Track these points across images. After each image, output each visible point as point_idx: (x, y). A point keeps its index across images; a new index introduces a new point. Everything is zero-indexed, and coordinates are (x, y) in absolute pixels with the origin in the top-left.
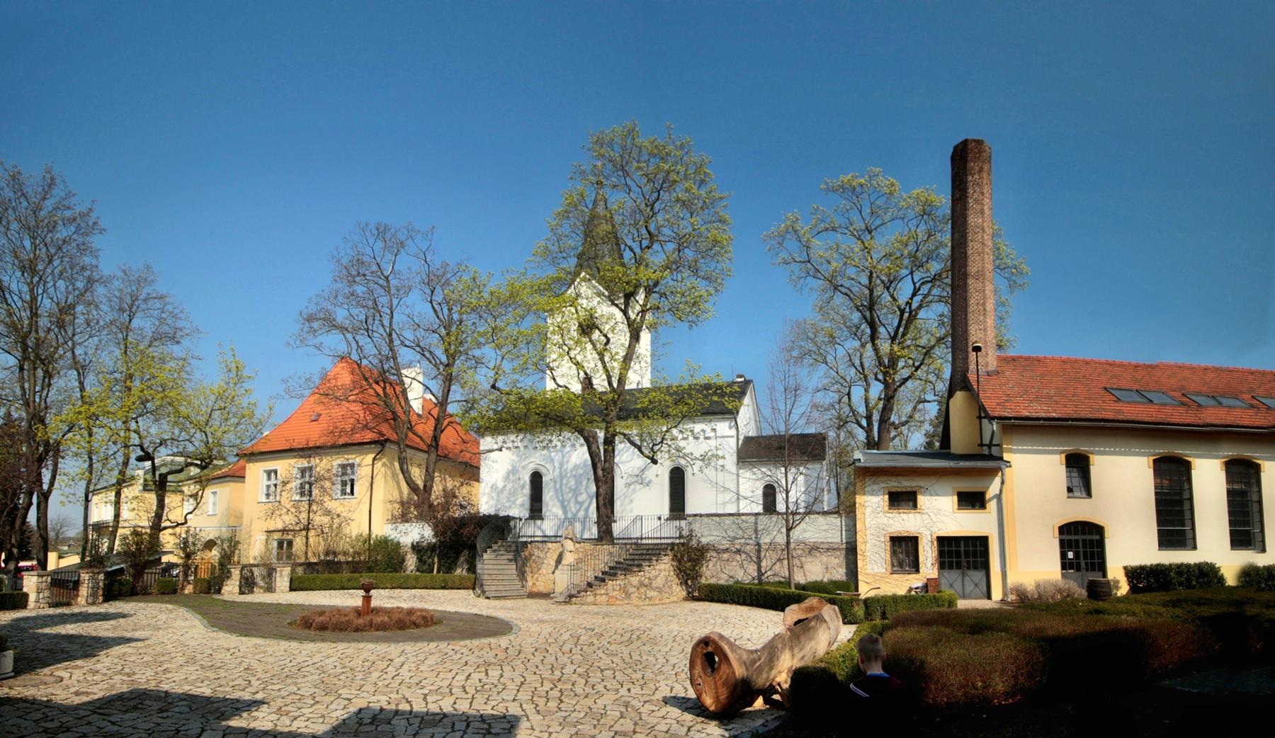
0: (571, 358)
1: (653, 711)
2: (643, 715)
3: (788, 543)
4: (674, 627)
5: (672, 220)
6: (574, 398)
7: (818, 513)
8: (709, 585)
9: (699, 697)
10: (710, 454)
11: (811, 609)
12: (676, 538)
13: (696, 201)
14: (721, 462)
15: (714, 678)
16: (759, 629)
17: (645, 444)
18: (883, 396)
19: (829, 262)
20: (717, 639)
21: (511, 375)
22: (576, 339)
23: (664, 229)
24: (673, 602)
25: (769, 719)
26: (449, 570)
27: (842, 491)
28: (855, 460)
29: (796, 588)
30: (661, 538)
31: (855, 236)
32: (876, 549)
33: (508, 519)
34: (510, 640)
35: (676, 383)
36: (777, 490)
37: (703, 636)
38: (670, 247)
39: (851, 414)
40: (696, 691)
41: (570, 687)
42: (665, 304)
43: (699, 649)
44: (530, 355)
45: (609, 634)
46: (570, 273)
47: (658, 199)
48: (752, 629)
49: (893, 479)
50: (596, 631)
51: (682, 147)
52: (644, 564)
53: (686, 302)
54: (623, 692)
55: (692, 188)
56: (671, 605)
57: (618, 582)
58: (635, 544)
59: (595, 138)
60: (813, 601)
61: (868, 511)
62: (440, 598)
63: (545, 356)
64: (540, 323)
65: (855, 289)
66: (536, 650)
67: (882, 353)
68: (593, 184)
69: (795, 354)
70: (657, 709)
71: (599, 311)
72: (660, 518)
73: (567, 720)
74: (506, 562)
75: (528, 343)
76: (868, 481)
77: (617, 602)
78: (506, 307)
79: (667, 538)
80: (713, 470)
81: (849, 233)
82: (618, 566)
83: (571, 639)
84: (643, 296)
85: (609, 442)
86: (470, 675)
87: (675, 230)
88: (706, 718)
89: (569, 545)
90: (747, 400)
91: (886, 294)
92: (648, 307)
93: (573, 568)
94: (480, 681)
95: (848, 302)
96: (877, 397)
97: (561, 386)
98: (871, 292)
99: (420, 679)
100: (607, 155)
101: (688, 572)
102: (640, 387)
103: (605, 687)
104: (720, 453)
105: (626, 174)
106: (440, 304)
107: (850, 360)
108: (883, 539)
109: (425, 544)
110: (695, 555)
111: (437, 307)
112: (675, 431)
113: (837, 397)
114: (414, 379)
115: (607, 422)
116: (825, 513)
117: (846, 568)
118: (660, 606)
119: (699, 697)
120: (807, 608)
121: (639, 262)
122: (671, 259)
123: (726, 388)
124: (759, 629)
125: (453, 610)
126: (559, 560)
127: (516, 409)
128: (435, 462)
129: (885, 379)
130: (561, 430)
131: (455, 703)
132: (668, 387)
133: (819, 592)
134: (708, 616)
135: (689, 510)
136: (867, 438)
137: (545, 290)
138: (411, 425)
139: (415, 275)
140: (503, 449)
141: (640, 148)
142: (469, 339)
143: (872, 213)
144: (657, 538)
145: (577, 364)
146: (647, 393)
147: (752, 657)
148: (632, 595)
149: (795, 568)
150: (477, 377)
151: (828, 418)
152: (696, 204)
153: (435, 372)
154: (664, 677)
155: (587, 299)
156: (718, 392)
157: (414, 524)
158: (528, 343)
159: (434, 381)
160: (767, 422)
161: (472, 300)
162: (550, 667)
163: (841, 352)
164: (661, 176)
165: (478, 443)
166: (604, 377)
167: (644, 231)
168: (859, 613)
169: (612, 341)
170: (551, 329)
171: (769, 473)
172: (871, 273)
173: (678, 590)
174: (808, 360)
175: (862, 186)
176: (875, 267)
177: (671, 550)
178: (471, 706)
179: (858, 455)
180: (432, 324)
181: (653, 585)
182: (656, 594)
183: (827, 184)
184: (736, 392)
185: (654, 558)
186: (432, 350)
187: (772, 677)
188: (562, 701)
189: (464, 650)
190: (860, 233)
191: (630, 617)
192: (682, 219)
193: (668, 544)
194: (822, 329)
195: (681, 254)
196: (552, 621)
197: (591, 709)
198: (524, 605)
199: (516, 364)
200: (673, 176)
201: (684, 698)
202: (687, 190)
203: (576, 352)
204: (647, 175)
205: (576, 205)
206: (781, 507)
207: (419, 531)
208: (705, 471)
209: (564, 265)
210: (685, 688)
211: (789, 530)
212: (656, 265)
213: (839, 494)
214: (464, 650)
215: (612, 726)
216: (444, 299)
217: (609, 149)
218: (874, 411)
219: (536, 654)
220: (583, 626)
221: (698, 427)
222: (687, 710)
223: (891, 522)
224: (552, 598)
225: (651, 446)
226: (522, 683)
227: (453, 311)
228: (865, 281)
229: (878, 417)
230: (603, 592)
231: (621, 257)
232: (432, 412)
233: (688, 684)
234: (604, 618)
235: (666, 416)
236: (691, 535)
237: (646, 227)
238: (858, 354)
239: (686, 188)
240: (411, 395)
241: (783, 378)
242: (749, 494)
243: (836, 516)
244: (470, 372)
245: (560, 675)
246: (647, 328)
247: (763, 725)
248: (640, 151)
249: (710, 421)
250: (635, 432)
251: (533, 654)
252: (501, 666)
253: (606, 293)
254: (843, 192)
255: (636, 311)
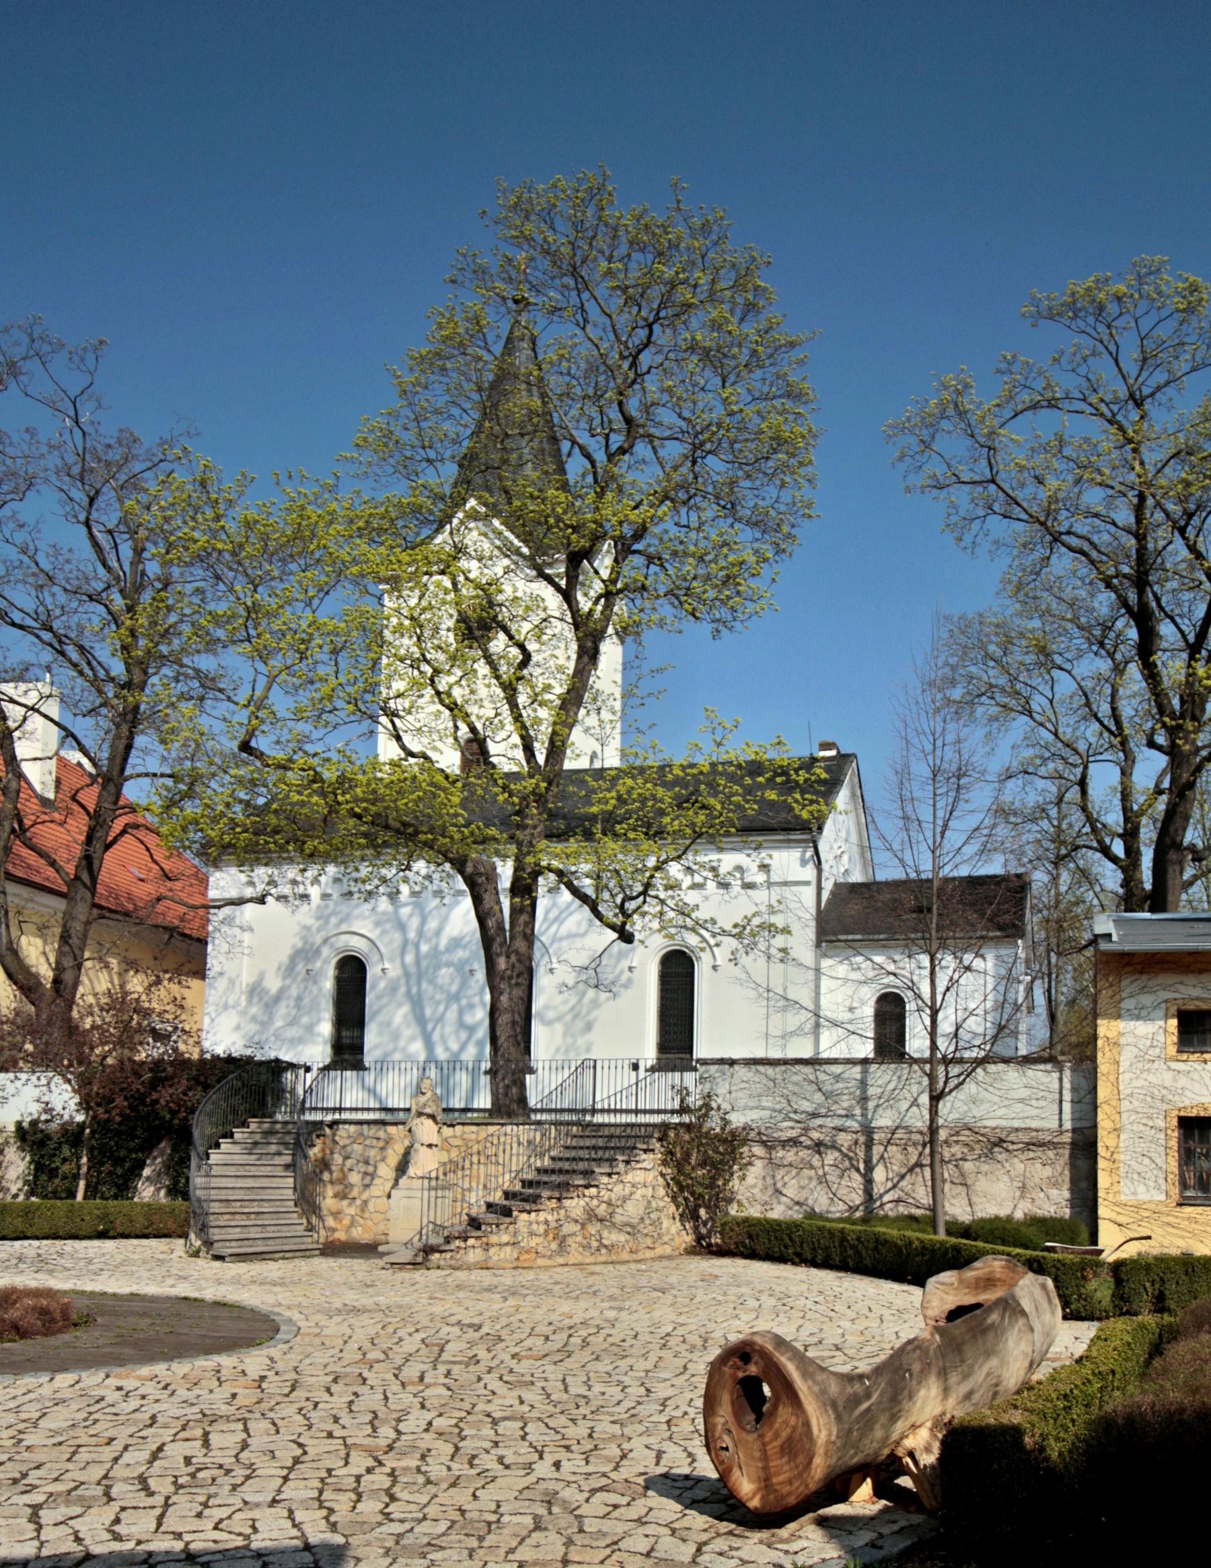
0: (438, 693)
1: (616, 1507)
2: (586, 1521)
3: (933, 1130)
4: (665, 1315)
5: (679, 391)
6: (445, 783)
7: (1006, 1061)
8: (746, 1220)
9: (724, 1477)
10: (756, 921)
11: (989, 1282)
12: (673, 1112)
13: (735, 350)
14: (779, 941)
15: (761, 1436)
16: (861, 1324)
17: (606, 895)
18: (1166, 784)
19: (1040, 481)
20: (770, 1347)
21: (291, 724)
22: (452, 649)
23: (660, 410)
24: (661, 1258)
25: (886, 1530)
26: (124, 1186)
27: (1062, 1011)
28: (1096, 936)
29: (949, 1233)
30: (637, 1112)
31: (1102, 415)
32: (1142, 1146)
33: (277, 1068)
34: (272, 1359)
35: (680, 759)
36: (910, 1006)
37: (734, 1338)
38: (674, 451)
39: (1087, 829)
40: (717, 1463)
41: (414, 1463)
42: (659, 580)
43: (727, 1370)
44: (342, 680)
45: (517, 1336)
46: (442, 498)
47: (648, 343)
48: (846, 1324)
49: (1191, 979)
50: (485, 1330)
51: (705, 228)
52: (597, 1170)
53: (708, 578)
54: (543, 1468)
55: (727, 321)
56: (657, 1265)
57: (542, 1216)
58: (578, 1123)
59: (513, 199)
60: (994, 1265)
61: (1126, 1057)
62: (90, 1262)
63: (377, 684)
64: (368, 605)
65: (1103, 538)
66: (335, 1381)
67: (1166, 683)
68: (504, 299)
69: (957, 693)
70: (624, 1501)
71: (508, 589)
72: (635, 1067)
73: (404, 1542)
74: (279, 1171)
75: (335, 652)
76: (1129, 985)
77: (540, 1262)
78: (283, 560)
79: (652, 1112)
80: (762, 960)
81: (1089, 410)
82: (545, 1178)
83: (424, 1351)
84: (608, 561)
85: (524, 888)
86: (160, 1449)
87: (686, 414)
88: (739, 1523)
89: (426, 1130)
90: (842, 798)
91: (1178, 542)
92: (619, 585)
93: (437, 1183)
94: (188, 1460)
95: (1084, 569)
96: (1152, 785)
97: (412, 755)
98: (1140, 538)
99: (24, 1469)
100: (539, 239)
101: (699, 1190)
102: (597, 765)
103: (501, 1460)
104: (779, 921)
105: (583, 284)
106: (110, 532)
107: (1088, 704)
108: (1161, 1123)
109: (54, 1126)
110: (716, 1151)
111: (101, 538)
112: (674, 869)
113: (1054, 789)
114: (32, 709)
115: (519, 844)
116: (1028, 1060)
117: (1072, 1190)
118: (633, 1266)
119: (724, 1477)
120: (978, 1279)
121: (602, 484)
122: (676, 477)
123: (796, 771)
124: (861, 1324)
125: (125, 1290)
126: (402, 1168)
127: (303, 804)
128: (88, 923)
129: (1173, 744)
130: (410, 857)
131: (117, 1521)
132: (662, 768)
133: (1004, 1242)
134: (743, 1290)
135: (701, 1049)
136: (1125, 884)
137: (381, 530)
138: (20, 823)
139: (44, 449)
140: (269, 899)
141: (615, 229)
142: (186, 629)
143: (1144, 360)
144: (628, 1111)
145: (453, 707)
146: (614, 780)
147: (849, 1390)
148: (570, 1241)
149: (947, 1186)
150: (204, 722)
151: (1031, 837)
152: (734, 357)
153: (92, 699)
154: (640, 1428)
155: (480, 560)
156: (779, 780)
157: (24, 1076)
158: (335, 652)
159: (90, 721)
160: (891, 849)
161: (196, 535)
162: (370, 1417)
163: (1065, 685)
164: (656, 292)
165: (204, 882)
166: (516, 739)
167: (614, 414)
168: (1099, 1295)
169: (535, 658)
170: (394, 621)
171: (891, 968)
172: (1142, 497)
173: (673, 1230)
174: (986, 708)
175: (1119, 299)
176: (1150, 485)
177: (660, 1140)
178: (159, 1525)
179: (1103, 924)
180: (87, 580)
181: (618, 1219)
182: (622, 1238)
183: (1036, 302)
184: (820, 782)
185: (620, 1158)
186: (87, 645)
187: (895, 1436)
188: (393, 1498)
189: (150, 1389)
190: (1115, 408)
191: (567, 1296)
192: (702, 389)
193: (654, 1126)
194: (1022, 635)
195: (697, 469)
196: (378, 1308)
197: (462, 1512)
198: (311, 1274)
199: (305, 697)
200: (684, 294)
201: (687, 1477)
202: (716, 326)
203: (452, 679)
204: (625, 289)
205: (461, 343)
206: (916, 1043)
207: (36, 1093)
208: (744, 960)
209: (429, 477)
210: (690, 1455)
211: (936, 1098)
212: (641, 491)
213: (1052, 1017)
214: (150, 1389)
215: (512, 1551)
216: (123, 520)
217: (544, 227)
218: (1144, 820)
219: (334, 1388)
220: (453, 1320)
221: (728, 861)
222: (693, 1504)
223: (1183, 1081)
224: (382, 1255)
225: (619, 900)
226: (297, 1461)
227: (146, 555)
228: (1125, 516)
229: (1154, 836)
230: (505, 1238)
231: (562, 470)
232: (80, 797)
233: (697, 1446)
234: (505, 1299)
235: (657, 834)
236: (707, 1106)
237: (620, 404)
238: (1108, 690)
239: (713, 321)
240: (22, 749)
241: (929, 747)
242: (844, 1016)
243: (1049, 1067)
244: (186, 707)
245: (393, 1435)
246: (617, 633)
247: (873, 1545)
248: (615, 237)
249: (758, 848)
250: (586, 867)
251: (328, 1390)
252: (245, 1421)
253: (525, 550)
254: (1076, 316)
255: (592, 594)
